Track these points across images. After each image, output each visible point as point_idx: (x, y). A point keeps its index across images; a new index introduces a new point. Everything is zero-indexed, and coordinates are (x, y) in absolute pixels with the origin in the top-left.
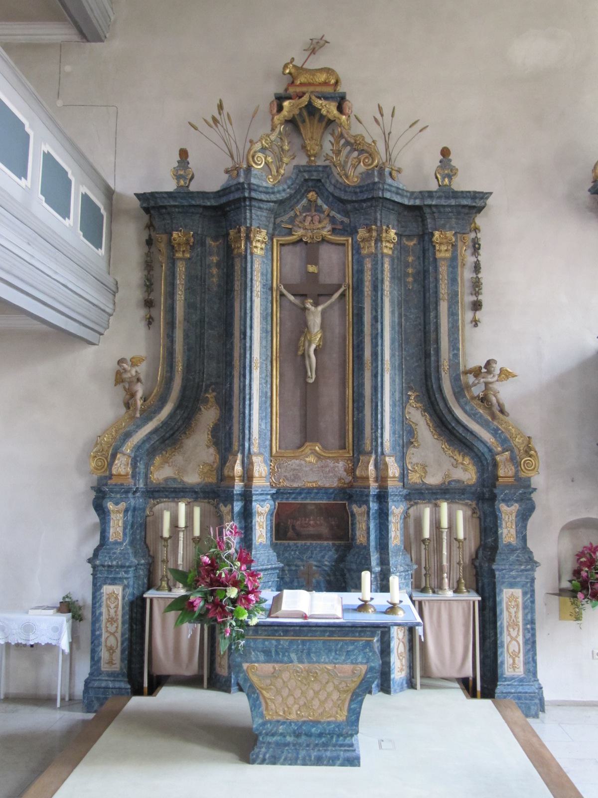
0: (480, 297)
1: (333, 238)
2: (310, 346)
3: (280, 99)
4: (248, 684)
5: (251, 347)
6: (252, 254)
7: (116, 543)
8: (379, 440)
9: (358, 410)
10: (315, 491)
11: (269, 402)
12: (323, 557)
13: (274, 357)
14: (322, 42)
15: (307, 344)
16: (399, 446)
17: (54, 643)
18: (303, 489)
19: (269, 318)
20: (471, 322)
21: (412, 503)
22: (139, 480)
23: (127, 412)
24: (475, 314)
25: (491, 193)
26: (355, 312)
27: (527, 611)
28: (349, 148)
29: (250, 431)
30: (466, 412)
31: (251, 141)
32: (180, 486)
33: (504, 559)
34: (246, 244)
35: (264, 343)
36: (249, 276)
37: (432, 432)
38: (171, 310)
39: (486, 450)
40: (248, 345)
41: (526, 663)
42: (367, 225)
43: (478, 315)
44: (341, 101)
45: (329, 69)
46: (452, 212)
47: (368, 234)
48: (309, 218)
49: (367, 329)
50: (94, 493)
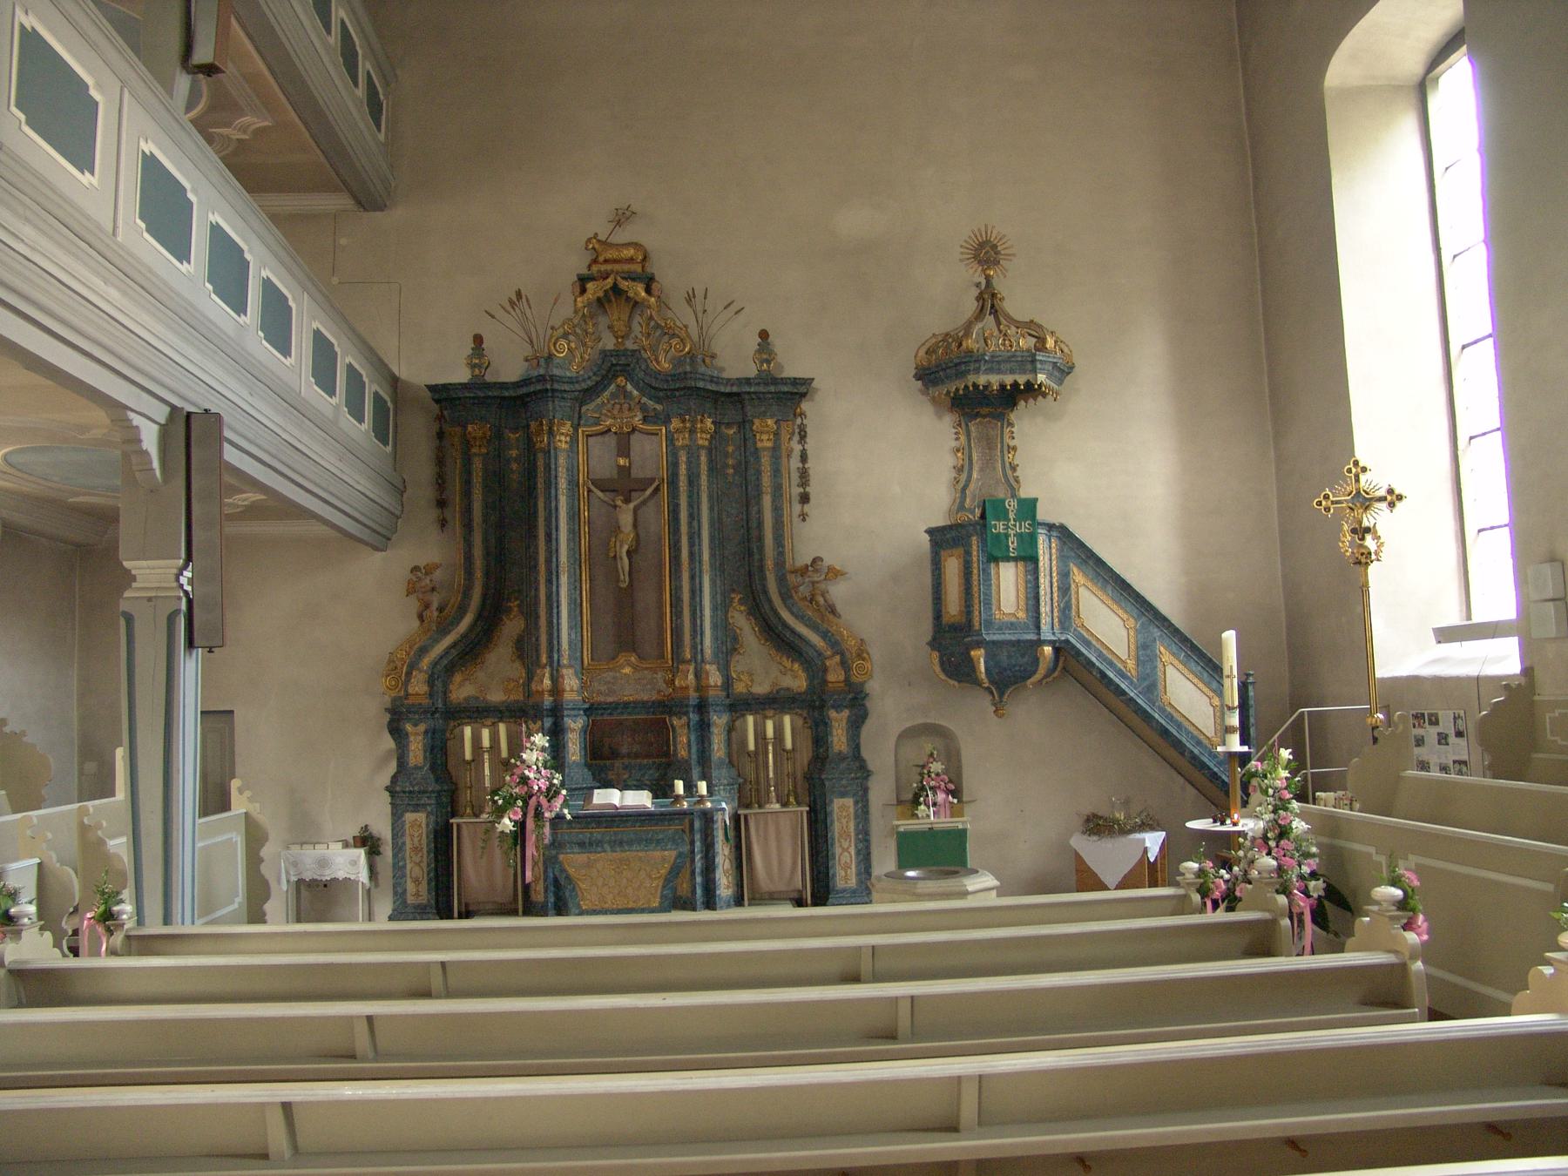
0: (808, 489)
1: (645, 427)
2: (621, 546)
3: (583, 281)
4: (564, 876)
5: (557, 550)
6: (555, 449)
7: (416, 768)
8: (699, 647)
12: (643, 775)
14: (628, 213)
15: (618, 544)
16: (723, 653)
17: (352, 877)
19: (576, 517)
20: (799, 516)
21: (738, 715)
22: (437, 700)
23: (421, 625)
24: (803, 507)
25: (813, 379)
26: (671, 508)
27: (858, 820)
28: (658, 332)
30: (792, 613)
31: (552, 328)
32: (483, 705)
33: (833, 768)
34: (549, 438)
36: (553, 473)
37: (758, 637)
38: (467, 510)
41: (858, 874)
43: (806, 508)
44: (649, 282)
45: (636, 244)
47: (682, 425)
48: (618, 406)
49: (684, 528)
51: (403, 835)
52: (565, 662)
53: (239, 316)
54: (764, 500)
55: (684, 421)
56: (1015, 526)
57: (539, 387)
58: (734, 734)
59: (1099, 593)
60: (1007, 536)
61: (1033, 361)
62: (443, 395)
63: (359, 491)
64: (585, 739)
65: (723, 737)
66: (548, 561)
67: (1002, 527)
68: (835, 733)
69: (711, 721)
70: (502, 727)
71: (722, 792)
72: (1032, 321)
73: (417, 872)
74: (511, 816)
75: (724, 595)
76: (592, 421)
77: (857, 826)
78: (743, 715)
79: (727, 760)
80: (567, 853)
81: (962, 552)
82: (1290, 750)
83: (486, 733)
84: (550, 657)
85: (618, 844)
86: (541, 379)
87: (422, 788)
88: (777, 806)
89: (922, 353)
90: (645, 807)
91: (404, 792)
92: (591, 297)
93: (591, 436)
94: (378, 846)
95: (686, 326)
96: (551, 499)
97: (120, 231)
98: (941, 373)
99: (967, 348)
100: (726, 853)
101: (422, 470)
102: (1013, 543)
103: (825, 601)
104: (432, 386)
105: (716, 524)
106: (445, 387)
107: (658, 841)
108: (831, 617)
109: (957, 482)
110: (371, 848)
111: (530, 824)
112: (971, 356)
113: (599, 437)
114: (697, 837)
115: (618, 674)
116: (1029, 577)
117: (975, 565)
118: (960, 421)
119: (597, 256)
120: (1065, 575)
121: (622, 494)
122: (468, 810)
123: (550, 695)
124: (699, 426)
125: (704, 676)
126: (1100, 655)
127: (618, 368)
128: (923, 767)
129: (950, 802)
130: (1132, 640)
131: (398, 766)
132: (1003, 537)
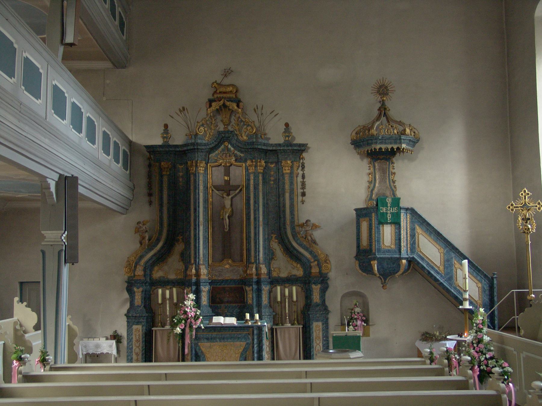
0: (305, 190)
2: (226, 214)
3: (210, 102)
4: (201, 351)
5: (199, 216)
6: (198, 173)
7: (138, 306)
9: (248, 243)
10: (229, 281)
11: (207, 241)
12: (233, 311)
13: (209, 220)
14: (230, 71)
15: (224, 213)
16: (267, 259)
17: (110, 352)
18: (223, 280)
21: (274, 286)
25: (307, 144)
27: (324, 332)
29: (199, 254)
30: (298, 244)
34: (196, 169)
35: (205, 213)
36: (197, 183)
38: (161, 198)
39: (307, 261)
40: (197, 215)
42: (251, 159)
44: (238, 102)
46: (290, 152)
48: (225, 155)
50: (126, 284)
51: (132, 335)
52: (201, 263)
53: (80, 134)
54: (286, 196)
55: (252, 162)
56: (390, 209)
57: (192, 147)
58: (272, 294)
59: (428, 238)
60: (387, 213)
61: (400, 139)
62: (151, 149)
63: (118, 193)
64: (209, 295)
65: (267, 295)
66: (195, 220)
67: (385, 210)
68: (314, 294)
69: (262, 289)
70: (174, 290)
71: (266, 318)
72: (400, 121)
73: (137, 350)
74: (180, 327)
75: (269, 235)
76: (214, 161)
77: (323, 334)
78: (276, 286)
79: (269, 305)
80: (202, 342)
81: (369, 219)
82: (484, 309)
83: (168, 292)
84: (195, 261)
85: (222, 339)
86: (193, 144)
87: (140, 315)
88: (289, 325)
89: (354, 134)
90: (234, 324)
91: (133, 317)
92: (214, 109)
93: (213, 167)
94: (121, 339)
95: (254, 122)
96: (196, 194)
97: (48, 117)
98: (361, 143)
99: (372, 133)
100: (268, 344)
101: (142, 181)
102: (389, 217)
103: (311, 238)
104: (147, 146)
105: (265, 206)
106: (152, 147)
107: (239, 338)
108: (314, 245)
109: (369, 188)
110: (117, 340)
111: (187, 330)
112: (373, 137)
113: (217, 168)
114: (255, 337)
115: (223, 268)
116: (396, 231)
117: (374, 225)
118: (371, 161)
119: (216, 90)
120: (413, 230)
121: (225, 192)
122: (159, 324)
123: (195, 277)
124: (259, 164)
125: (259, 269)
126: (428, 264)
127: (225, 138)
128: (352, 309)
129: (363, 325)
130: (442, 258)
131: (130, 305)
132: (385, 214)
